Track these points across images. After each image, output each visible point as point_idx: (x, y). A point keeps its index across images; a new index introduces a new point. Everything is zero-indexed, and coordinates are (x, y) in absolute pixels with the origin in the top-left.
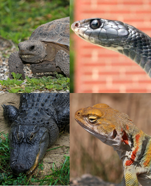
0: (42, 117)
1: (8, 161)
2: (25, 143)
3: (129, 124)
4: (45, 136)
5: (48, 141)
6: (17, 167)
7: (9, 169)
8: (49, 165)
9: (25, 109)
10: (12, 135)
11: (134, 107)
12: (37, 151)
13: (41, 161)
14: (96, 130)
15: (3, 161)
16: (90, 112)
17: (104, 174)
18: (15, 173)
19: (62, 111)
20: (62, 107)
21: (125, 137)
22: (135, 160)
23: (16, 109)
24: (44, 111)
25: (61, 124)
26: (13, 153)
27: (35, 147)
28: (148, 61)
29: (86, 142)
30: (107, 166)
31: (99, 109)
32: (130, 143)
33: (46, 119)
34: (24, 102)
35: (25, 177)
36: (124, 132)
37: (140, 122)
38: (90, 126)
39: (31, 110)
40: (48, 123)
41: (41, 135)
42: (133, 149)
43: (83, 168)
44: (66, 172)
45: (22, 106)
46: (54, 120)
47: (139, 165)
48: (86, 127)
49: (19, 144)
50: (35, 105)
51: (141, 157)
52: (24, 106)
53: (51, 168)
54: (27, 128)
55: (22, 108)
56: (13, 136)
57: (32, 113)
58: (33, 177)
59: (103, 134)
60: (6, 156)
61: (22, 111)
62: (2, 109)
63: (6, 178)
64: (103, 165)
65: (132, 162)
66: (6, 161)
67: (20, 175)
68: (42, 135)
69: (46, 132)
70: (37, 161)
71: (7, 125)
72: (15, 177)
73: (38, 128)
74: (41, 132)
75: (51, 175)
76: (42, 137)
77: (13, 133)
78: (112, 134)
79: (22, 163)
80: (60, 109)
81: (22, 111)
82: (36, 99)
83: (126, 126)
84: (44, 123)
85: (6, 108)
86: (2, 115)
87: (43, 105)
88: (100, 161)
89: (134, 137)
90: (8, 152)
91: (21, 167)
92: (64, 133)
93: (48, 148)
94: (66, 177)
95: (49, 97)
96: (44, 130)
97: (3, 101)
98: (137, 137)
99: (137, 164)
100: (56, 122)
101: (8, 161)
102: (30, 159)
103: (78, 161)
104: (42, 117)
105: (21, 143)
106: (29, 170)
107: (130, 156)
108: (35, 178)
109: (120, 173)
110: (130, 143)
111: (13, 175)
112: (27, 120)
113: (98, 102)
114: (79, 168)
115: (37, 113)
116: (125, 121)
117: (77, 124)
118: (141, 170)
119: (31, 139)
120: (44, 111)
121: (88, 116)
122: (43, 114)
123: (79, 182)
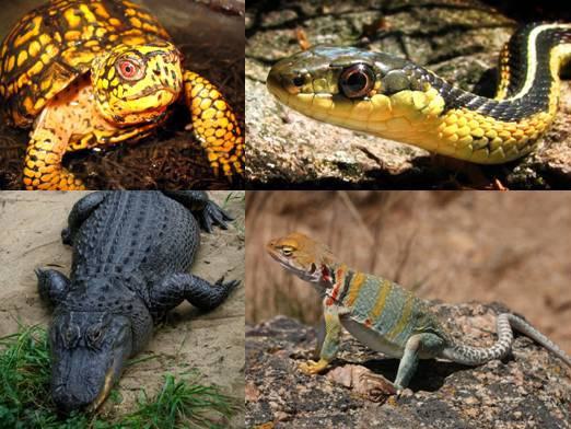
0: (117, 294)
1: (48, 386)
2: (81, 347)
3: (330, 257)
4: (123, 333)
5: (130, 343)
6: (66, 398)
7: (50, 402)
8: (132, 393)
9: (83, 278)
10: (55, 331)
11: (335, 237)
12: (107, 365)
13: (115, 385)
14: (292, 264)
15: (37, 385)
16: (284, 243)
17: (301, 315)
18: (62, 410)
19: (159, 282)
20: (158, 273)
21: (325, 272)
22: (337, 298)
23: (63, 277)
24: (121, 283)
25: (158, 309)
26: (58, 370)
27: (103, 356)
28: (369, 49)
29: (280, 278)
30: (304, 305)
31: (295, 240)
32: (331, 279)
33: (127, 298)
34: (81, 264)
35: (83, 418)
36: (324, 266)
37: (343, 254)
38: (284, 259)
39: (94, 280)
40: (130, 307)
41: (115, 331)
42: (335, 286)
43: (277, 307)
44: (167, 407)
45: (77, 272)
46: (143, 300)
47: (341, 304)
48: (280, 261)
49: (71, 350)
50: (102, 270)
51: (343, 295)
52: (80, 271)
53: (137, 401)
54: (87, 316)
55: (77, 276)
56: (57, 334)
57: (98, 287)
58: (99, 418)
59: (300, 268)
60: (43, 375)
61: (77, 283)
62: (35, 278)
63: (44, 421)
64: (300, 305)
65: (333, 300)
66: (44, 385)
67: (72, 414)
68: (116, 333)
69: (127, 325)
70: (106, 386)
71: (45, 311)
72: (62, 417)
73: (110, 317)
74: (117, 325)
75: (136, 414)
76: (117, 338)
77: (57, 328)
78: (310, 269)
79: (76, 390)
80: (155, 277)
81: (77, 283)
82: (105, 258)
83: (326, 259)
84: (121, 308)
85: (43, 277)
86: (36, 289)
87: (119, 270)
88: (296, 300)
89: (335, 272)
90: (47, 367)
91: (74, 397)
92: (162, 327)
93: (131, 357)
94: (167, 418)
95: (131, 254)
96: (122, 321)
97: (37, 261)
98: (339, 272)
99: (339, 303)
100: (146, 305)
101: (48, 386)
102: (93, 381)
103: (271, 299)
104: (117, 294)
105: (75, 349)
106: (91, 403)
107: (331, 295)
108: (103, 420)
109: (319, 313)
110: (331, 279)
111: (59, 415)
112: (87, 302)
113: (294, 232)
114: (272, 308)
115: (108, 287)
116: (326, 254)
117: (269, 257)
118: (344, 310)
119: (94, 339)
120: (121, 283)
121: (282, 247)
122: (118, 287)
123: (272, 324)
